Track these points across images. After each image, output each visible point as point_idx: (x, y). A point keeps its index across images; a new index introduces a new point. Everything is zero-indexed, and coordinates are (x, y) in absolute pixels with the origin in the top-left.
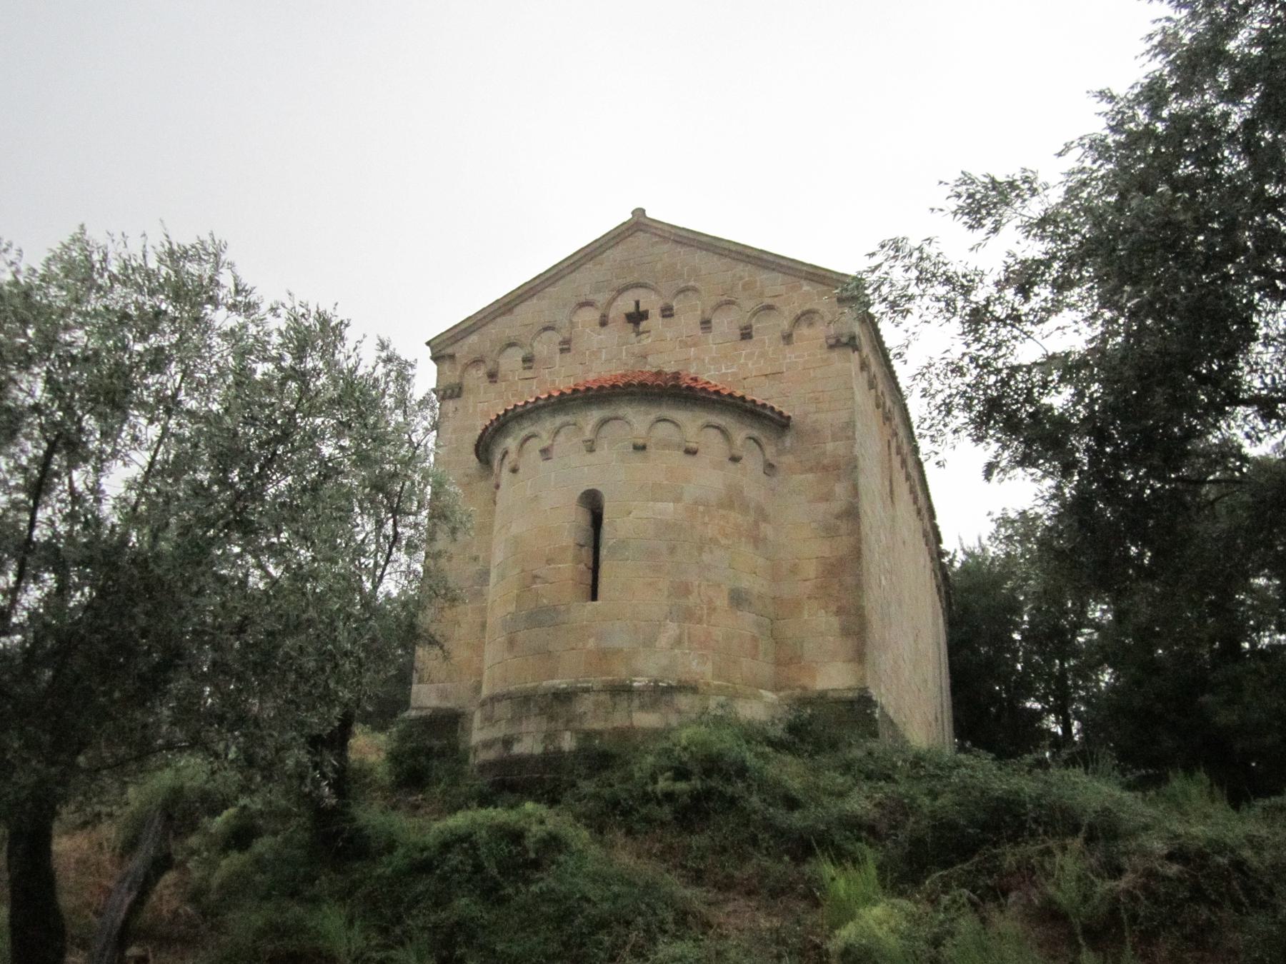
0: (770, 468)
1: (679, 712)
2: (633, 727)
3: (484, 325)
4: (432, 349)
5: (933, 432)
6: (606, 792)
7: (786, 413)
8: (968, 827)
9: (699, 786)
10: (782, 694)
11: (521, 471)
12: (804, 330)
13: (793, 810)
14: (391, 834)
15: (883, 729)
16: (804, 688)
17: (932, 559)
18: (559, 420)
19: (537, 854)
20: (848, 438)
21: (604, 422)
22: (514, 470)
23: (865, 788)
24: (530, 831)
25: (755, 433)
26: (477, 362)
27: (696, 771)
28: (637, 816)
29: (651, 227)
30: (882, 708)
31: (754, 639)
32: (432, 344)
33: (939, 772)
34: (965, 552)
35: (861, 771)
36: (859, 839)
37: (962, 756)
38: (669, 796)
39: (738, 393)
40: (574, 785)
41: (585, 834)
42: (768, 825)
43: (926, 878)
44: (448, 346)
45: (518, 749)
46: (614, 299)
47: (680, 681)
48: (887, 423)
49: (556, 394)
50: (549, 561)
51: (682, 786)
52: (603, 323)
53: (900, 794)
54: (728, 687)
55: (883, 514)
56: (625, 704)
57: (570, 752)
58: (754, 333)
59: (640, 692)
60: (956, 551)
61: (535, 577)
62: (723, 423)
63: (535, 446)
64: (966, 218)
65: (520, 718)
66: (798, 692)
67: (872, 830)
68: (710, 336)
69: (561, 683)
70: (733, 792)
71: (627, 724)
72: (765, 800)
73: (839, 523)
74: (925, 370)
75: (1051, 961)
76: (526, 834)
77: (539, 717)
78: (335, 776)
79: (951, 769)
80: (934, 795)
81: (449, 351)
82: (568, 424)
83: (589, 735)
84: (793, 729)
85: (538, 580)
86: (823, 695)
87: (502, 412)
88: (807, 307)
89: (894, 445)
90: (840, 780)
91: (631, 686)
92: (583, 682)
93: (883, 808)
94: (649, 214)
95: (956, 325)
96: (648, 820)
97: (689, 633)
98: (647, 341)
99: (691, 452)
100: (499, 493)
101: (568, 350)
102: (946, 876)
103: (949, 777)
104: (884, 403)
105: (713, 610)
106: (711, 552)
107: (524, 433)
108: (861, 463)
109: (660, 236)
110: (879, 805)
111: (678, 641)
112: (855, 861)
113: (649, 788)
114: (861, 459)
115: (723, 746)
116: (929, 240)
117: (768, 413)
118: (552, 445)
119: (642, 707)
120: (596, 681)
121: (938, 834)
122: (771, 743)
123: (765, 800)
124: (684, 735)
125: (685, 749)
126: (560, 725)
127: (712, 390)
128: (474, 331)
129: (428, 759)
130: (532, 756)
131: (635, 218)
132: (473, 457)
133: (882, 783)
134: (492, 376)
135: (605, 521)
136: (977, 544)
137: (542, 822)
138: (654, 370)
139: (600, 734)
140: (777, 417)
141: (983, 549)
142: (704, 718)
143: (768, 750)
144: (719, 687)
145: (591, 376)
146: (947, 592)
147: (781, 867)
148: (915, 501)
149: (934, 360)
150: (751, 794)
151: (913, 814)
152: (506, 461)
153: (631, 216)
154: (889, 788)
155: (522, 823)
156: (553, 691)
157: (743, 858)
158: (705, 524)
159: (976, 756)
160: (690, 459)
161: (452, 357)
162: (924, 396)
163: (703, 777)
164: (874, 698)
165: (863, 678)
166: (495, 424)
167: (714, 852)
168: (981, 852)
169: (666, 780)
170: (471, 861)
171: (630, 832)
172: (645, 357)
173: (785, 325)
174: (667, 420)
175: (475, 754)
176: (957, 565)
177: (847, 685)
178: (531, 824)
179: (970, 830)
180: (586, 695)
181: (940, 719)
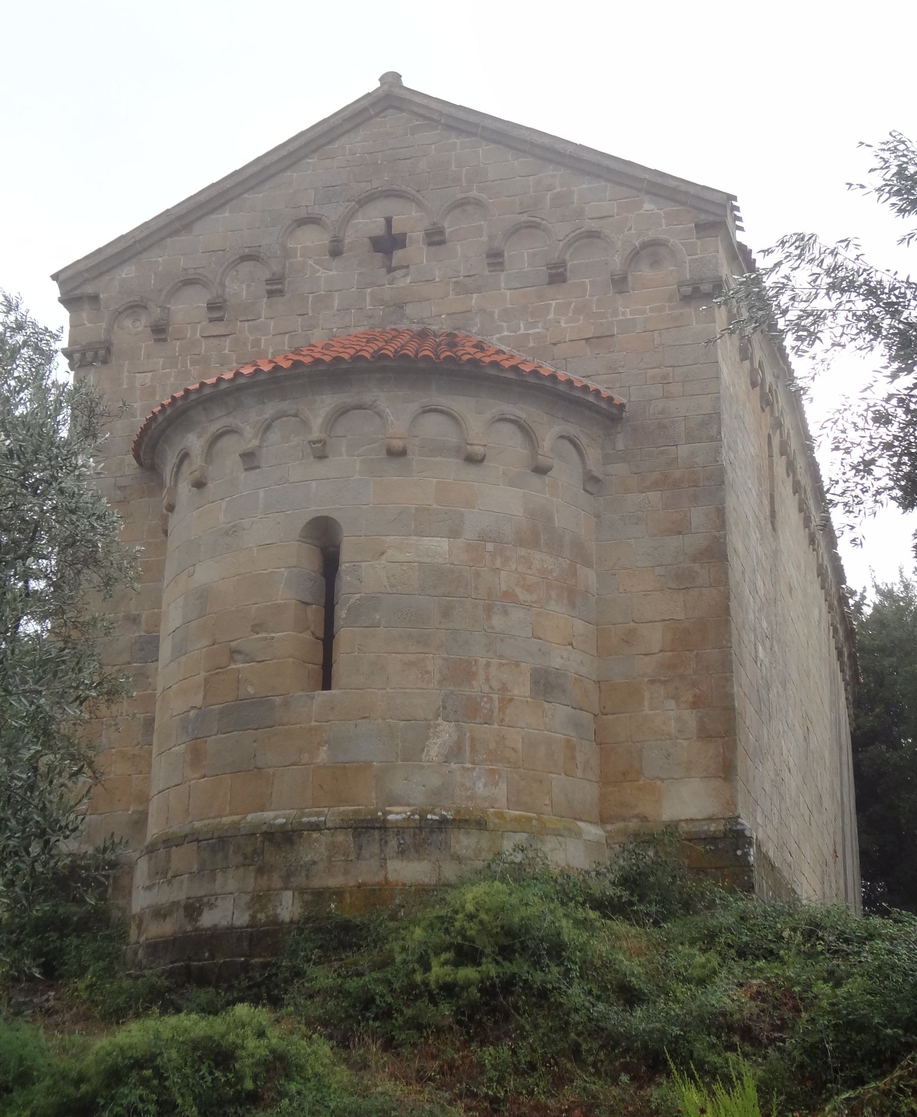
0: (592, 483)
1: (459, 859)
2: (387, 882)
3: (145, 250)
4: (61, 285)
5: (848, 498)
6: (352, 984)
7: (618, 399)
8: (885, 1027)
9: (493, 973)
10: (609, 827)
11: (210, 485)
12: (646, 272)
13: (632, 1007)
14: (21, 1059)
15: (759, 877)
16: (644, 819)
17: (831, 607)
18: (270, 409)
19: (255, 1081)
20: (711, 439)
21: (343, 412)
22: (199, 484)
23: (737, 971)
24: (243, 1048)
25: (571, 429)
26: (136, 308)
27: (488, 950)
28: (400, 1019)
29: (410, 101)
30: (759, 847)
31: (570, 746)
32: (61, 277)
33: (845, 947)
34: (879, 591)
35: (729, 946)
36: (732, 1047)
37: (876, 921)
38: (449, 989)
39: (547, 369)
40: (298, 974)
41: (325, 1049)
42: (596, 1030)
43: (827, 1101)
44: (85, 282)
45: (208, 919)
46: (352, 215)
47: (458, 812)
48: (768, 409)
49: (266, 368)
50: (257, 628)
51: (468, 973)
52: (336, 251)
53: (788, 979)
54: (530, 819)
55: (759, 549)
56: (375, 848)
57: (292, 922)
58: (568, 274)
59: (400, 829)
60: (865, 590)
61: (234, 652)
62: (523, 415)
63: (231, 447)
64: (894, 200)
65: (213, 871)
66: (633, 825)
67: (747, 1033)
68: (502, 276)
69: (277, 816)
70: (543, 981)
71: (379, 878)
72: (590, 992)
73: (697, 567)
74: (837, 416)
76: (239, 1052)
77: (241, 870)
79: (862, 941)
80: (835, 979)
81: (89, 289)
82: (284, 414)
83: (320, 895)
84: (626, 881)
85: (238, 657)
86: (671, 828)
87: (179, 394)
88: (651, 235)
89: (776, 442)
90: (700, 959)
91: (385, 821)
92: (310, 815)
93: (764, 1001)
94: (407, 82)
95: (880, 352)
96: (418, 1026)
97: (473, 739)
98: (404, 282)
99: (472, 460)
100: (174, 520)
101: (281, 292)
102: (856, 1098)
103: (858, 954)
104: (763, 380)
105: (507, 701)
106: (506, 613)
107: (215, 427)
108: (730, 476)
109: (424, 117)
110: (758, 995)
111: (455, 753)
112: (727, 1081)
113: (418, 978)
114: (729, 469)
115: (530, 911)
116: (847, 241)
117: (591, 399)
118: (260, 447)
119: (402, 853)
120: (330, 814)
121: (842, 1038)
122: (598, 905)
123: (590, 992)
124: (471, 896)
125: (471, 917)
126: (277, 882)
127: (507, 364)
128: (130, 258)
129: (62, 937)
130: (231, 929)
131: (386, 87)
132: (130, 459)
133: (761, 963)
134: (159, 331)
135: (344, 567)
136: (897, 579)
137: (261, 1034)
138: (416, 328)
139: (338, 893)
140: (603, 405)
141: (907, 587)
142: (498, 868)
143: (593, 915)
144: (517, 819)
145: (318, 337)
146: (852, 656)
147: (615, 1091)
148: (807, 521)
149: (850, 401)
150: (570, 984)
151: (806, 1010)
152: (185, 468)
153: (378, 84)
154: (772, 970)
155: (231, 1038)
156: (264, 828)
157: (560, 1080)
158: (497, 570)
159: (896, 921)
160: (473, 471)
161: (94, 299)
162: (837, 448)
163: (499, 958)
164: (747, 833)
165: (731, 803)
166: (169, 412)
167: (517, 1072)
168: (904, 1063)
169: (445, 963)
170: (155, 1097)
171: (389, 1044)
172: (400, 306)
173: (617, 261)
174: (442, 412)
175: (139, 927)
176: (867, 611)
177: (705, 814)
178: (244, 1038)
179: (889, 1031)
180: (315, 835)
181: (840, 854)
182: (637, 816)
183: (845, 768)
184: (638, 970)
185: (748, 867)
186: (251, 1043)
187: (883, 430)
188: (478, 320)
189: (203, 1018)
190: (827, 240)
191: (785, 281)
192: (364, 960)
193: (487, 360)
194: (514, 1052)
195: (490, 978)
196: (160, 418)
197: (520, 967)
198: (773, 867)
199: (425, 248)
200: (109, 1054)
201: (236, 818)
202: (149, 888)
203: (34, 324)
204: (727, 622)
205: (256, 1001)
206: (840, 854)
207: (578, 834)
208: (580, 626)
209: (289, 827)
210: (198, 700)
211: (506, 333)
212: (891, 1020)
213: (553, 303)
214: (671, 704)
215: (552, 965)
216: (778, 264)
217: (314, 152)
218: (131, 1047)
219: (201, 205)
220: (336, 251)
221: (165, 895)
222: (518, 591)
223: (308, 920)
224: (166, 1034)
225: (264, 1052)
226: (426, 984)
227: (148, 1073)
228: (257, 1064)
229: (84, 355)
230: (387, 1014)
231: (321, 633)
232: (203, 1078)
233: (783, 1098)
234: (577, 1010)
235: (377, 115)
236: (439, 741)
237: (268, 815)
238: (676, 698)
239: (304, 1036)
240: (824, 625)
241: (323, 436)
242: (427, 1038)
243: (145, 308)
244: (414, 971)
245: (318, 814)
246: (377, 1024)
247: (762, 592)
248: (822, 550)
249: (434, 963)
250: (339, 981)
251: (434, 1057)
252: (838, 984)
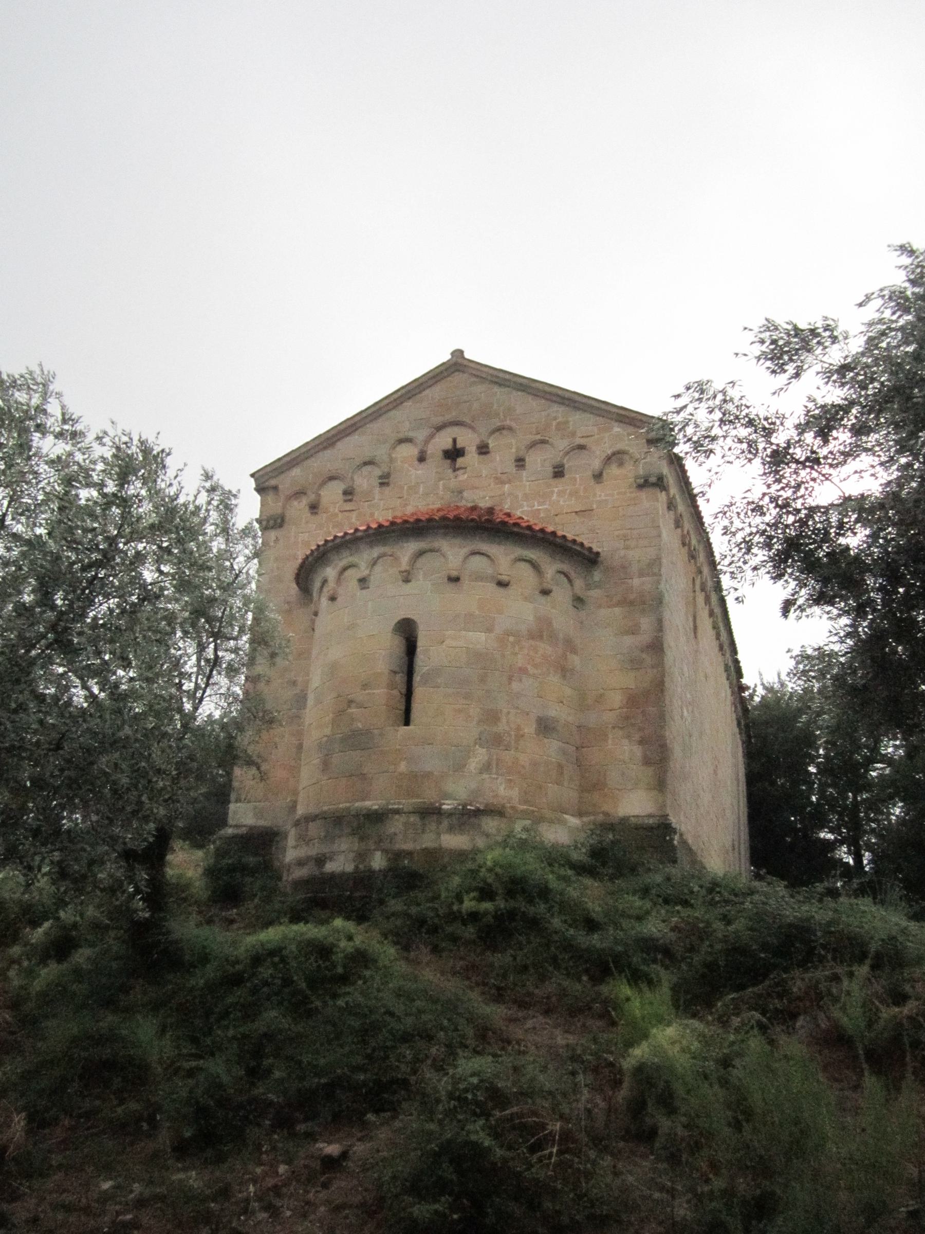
0: (579, 601)
6: (414, 910)
7: (595, 549)
10: (585, 819)
15: (680, 854)
16: (606, 814)
17: (733, 693)
18: (376, 551)
20: (654, 574)
21: (421, 553)
22: (333, 599)
23: (663, 911)
25: (565, 567)
26: (300, 494)
30: (681, 835)
31: (560, 766)
32: (256, 475)
34: (765, 688)
36: (655, 961)
37: (756, 884)
38: (474, 916)
39: (550, 529)
41: (392, 951)
42: (568, 946)
44: (272, 477)
45: (330, 867)
46: (432, 436)
48: (692, 561)
49: (374, 526)
50: (365, 686)
51: (487, 906)
52: (422, 459)
53: (697, 918)
54: (533, 812)
55: (686, 648)
59: (450, 814)
60: (756, 686)
61: (351, 702)
62: (533, 556)
66: (600, 818)
67: (667, 952)
68: (524, 473)
69: (372, 804)
73: (644, 656)
74: (726, 509)
79: (745, 895)
80: (727, 920)
81: (273, 482)
83: (398, 855)
86: (624, 820)
89: (698, 582)
90: (638, 903)
91: (440, 809)
92: (395, 804)
94: (467, 355)
98: (463, 477)
99: (502, 584)
103: (743, 903)
105: (520, 737)
108: (667, 598)
111: (486, 768)
112: (650, 982)
113: (455, 908)
115: (530, 867)
116: (733, 383)
117: (578, 548)
118: (369, 575)
119: (451, 829)
120: (406, 803)
124: (490, 858)
125: (490, 870)
127: (524, 525)
130: (343, 874)
131: (454, 359)
133: (678, 908)
134: (314, 507)
138: (470, 505)
139: (410, 854)
140: (586, 553)
142: (511, 841)
143: (570, 872)
145: (410, 510)
146: (747, 726)
147: (578, 987)
148: (718, 636)
150: (552, 915)
152: (325, 590)
153: (450, 357)
154: (685, 912)
155: (331, 939)
156: (364, 812)
157: (543, 978)
160: (501, 590)
164: (674, 825)
165: (663, 806)
168: (772, 976)
171: (436, 950)
172: (461, 492)
173: (596, 464)
174: (483, 554)
175: (288, 870)
176: (757, 699)
180: (397, 817)
181: (736, 847)
182: (603, 813)
183: (741, 794)
184: (598, 909)
185: (674, 848)
186: (343, 944)
187: (758, 519)
188: (509, 500)
189: (315, 927)
190: (718, 385)
191: (690, 417)
192: (420, 895)
193: (511, 522)
194: (515, 959)
195: (500, 909)
196: (310, 559)
197: (520, 904)
198: (690, 849)
199: (477, 456)
200: (254, 946)
201: (348, 805)
202: (295, 847)
203: (223, 488)
204: (662, 691)
205: (348, 918)
206: (736, 847)
207: (563, 822)
208: (568, 691)
209: (380, 811)
210: (328, 731)
211: (526, 508)
212: (765, 947)
213: (556, 490)
214: (625, 742)
215: (541, 903)
216: (685, 407)
217: (409, 398)
218: (268, 942)
219: (340, 432)
220: (422, 459)
221: (303, 852)
222: (529, 667)
223: (390, 870)
224: (291, 935)
225: (350, 950)
226: (460, 912)
227: (276, 959)
228: (346, 957)
229: (268, 521)
230: (434, 930)
231: (404, 691)
232: (311, 964)
233: (689, 997)
234: (556, 933)
235: (448, 376)
236: (477, 760)
237: (368, 803)
238: (628, 737)
239: (379, 942)
240: (729, 703)
241: (408, 568)
242: (459, 947)
243: (305, 494)
244: (453, 903)
245: (399, 803)
246: (427, 936)
247: (687, 675)
248: (728, 655)
249: (466, 898)
250: (405, 908)
251: (461, 958)
252: (729, 923)
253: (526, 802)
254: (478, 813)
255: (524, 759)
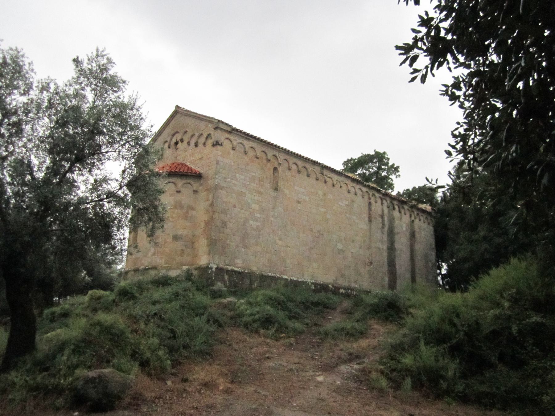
59: (141, 270)
75: (510, 415)
78: (462, 155)
105: (166, 242)
111: (154, 254)
253: (166, 263)
254: (149, 269)
255: (167, 250)
